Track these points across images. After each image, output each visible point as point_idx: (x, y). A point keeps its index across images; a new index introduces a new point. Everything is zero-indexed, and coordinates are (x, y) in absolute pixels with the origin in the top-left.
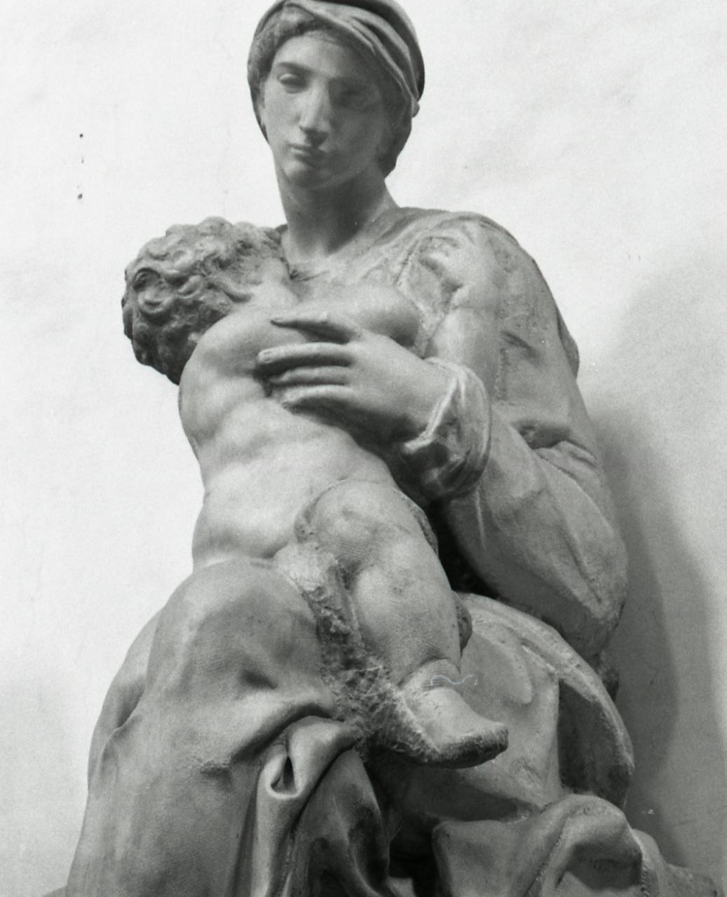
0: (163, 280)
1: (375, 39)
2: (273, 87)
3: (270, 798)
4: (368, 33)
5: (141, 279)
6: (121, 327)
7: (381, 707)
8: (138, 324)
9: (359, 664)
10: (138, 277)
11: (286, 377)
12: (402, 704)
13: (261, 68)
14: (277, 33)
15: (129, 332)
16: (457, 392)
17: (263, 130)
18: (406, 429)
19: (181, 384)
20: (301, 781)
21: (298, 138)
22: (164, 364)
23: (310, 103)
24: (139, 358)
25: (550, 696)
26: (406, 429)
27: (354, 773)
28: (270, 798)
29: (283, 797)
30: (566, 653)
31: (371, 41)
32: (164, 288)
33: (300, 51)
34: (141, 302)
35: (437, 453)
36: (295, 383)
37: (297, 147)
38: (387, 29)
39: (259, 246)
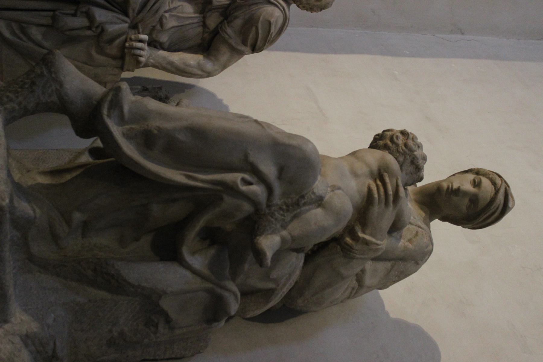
0: (405, 141)
1: (494, 210)
2: (471, 177)
3: (236, 177)
4: (496, 208)
5: (404, 133)
6: (386, 129)
7: (272, 219)
8: (389, 133)
9: (288, 211)
10: (405, 132)
11: (379, 183)
12: (413, 220)
13: (477, 172)
14: (491, 176)
15: (384, 131)
16: (378, 245)
17: (454, 175)
18: (364, 225)
19: (368, 149)
20: (244, 188)
21: (455, 186)
22: (375, 144)
23: (468, 187)
24: (376, 135)
25: (271, 285)
26: (364, 225)
27: (247, 208)
28: (236, 177)
29: (239, 182)
30: (285, 290)
31: (493, 209)
32: (403, 141)
33: (486, 182)
34: (397, 134)
35: (356, 238)
36: (377, 186)
37: (452, 186)
38: (496, 215)
39: (418, 174)
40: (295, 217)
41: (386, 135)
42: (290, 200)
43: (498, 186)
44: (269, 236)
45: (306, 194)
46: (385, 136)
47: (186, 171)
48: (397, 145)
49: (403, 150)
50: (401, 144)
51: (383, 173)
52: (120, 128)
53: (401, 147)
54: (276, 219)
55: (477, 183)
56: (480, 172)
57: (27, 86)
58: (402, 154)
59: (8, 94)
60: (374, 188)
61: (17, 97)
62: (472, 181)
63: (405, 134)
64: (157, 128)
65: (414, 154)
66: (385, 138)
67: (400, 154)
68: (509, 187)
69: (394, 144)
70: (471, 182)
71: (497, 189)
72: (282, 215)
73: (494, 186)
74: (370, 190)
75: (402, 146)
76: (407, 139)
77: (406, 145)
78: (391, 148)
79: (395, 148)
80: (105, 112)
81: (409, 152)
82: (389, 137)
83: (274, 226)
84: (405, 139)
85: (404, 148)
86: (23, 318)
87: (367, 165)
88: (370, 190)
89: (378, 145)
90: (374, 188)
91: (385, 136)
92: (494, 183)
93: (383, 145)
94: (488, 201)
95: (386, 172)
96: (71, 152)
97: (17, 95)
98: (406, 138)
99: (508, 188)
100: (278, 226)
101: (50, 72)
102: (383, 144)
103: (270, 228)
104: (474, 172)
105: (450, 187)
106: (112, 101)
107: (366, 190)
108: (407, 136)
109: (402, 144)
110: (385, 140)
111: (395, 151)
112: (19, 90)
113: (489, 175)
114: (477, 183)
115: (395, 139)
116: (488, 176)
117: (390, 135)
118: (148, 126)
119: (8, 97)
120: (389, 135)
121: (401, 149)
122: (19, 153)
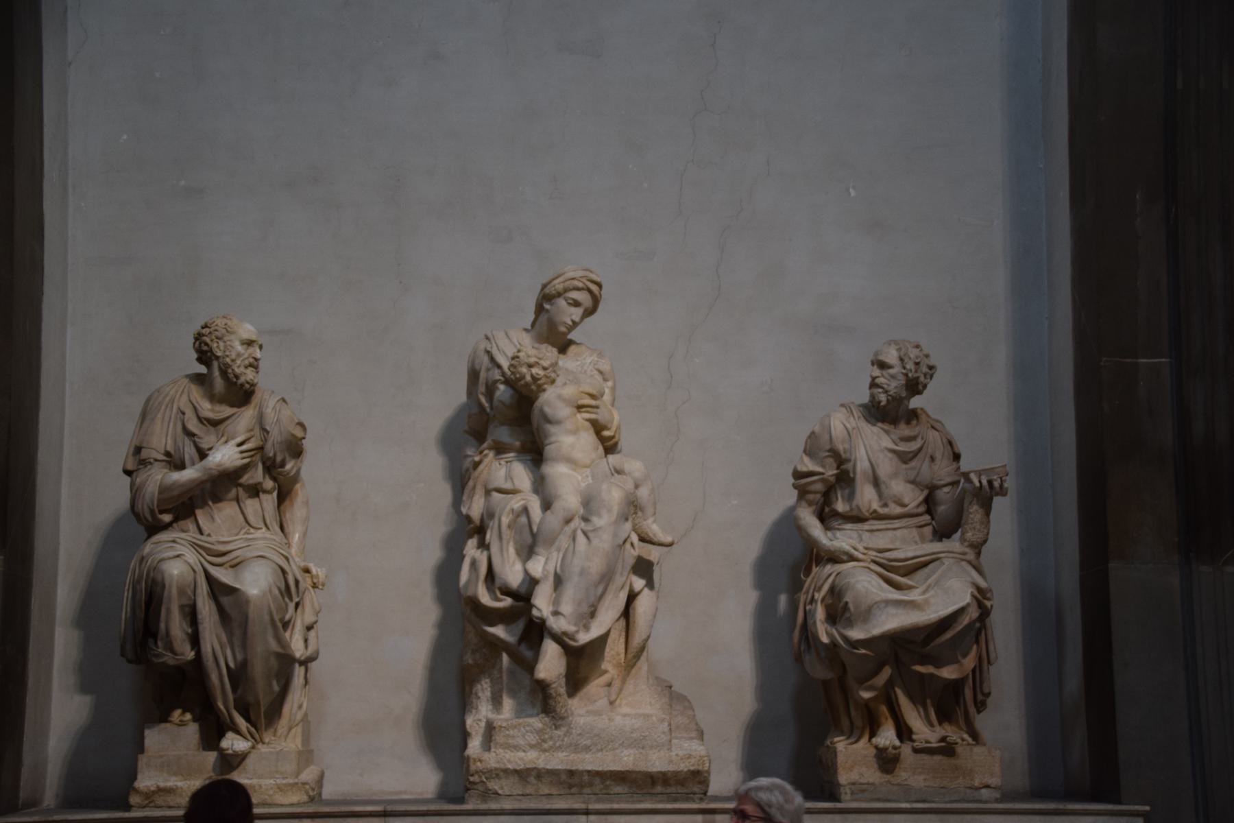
43: (585, 287)
74: (589, 420)
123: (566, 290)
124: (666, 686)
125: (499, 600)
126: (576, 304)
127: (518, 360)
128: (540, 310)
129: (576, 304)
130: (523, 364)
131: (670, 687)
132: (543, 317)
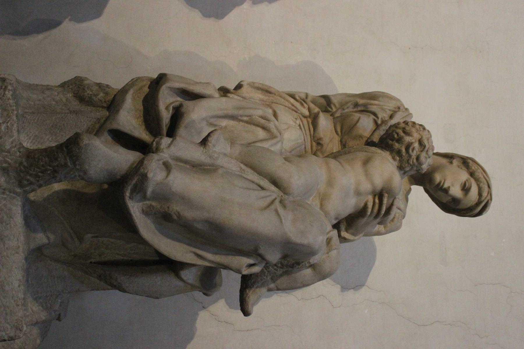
9: (281, 268)
10: (423, 143)
11: (377, 201)
40: (286, 273)
41: (405, 141)
42: (286, 262)
43: (483, 198)
44: (258, 290)
45: (302, 262)
46: (403, 141)
47: (195, 247)
48: (410, 156)
49: (413, 162)
50: (414, 156)
51: (384, 193)
52: (141, 204)
53: (412, 159)
54: (269, 272)
55: (466, 188)
56: (475, 175)
57: (49, 172)
58: (411, 165)
59: (28, 177)
60: (370, 205)
61: (38, 181)
62: (463, 184)
63: (422, 146)
64: (177, 213)
65: (421, 167)
66: (402, 143)
67: (409, 165)
68: (491, 200)
69: (407, 154)
70: (461, 184)
71: (480, 201)
72: (275, 269)
73: (479, 197)
74: (365, 206)
75: (413, 159)
76: (422, 151)
77: (418, 158)
78: (403, 157)
79: (406, 158)
80: (128, 194)
81: (418, 164)
82: (406, 143)
83: (265, 277)
84: (419, 150)
85: (415, 161)
86: (34, 308)
87: (373, 184)
88: (365, 206)
89: (393, 147)
90: (370, 205)
91: (403, 141)
92: (480, 194)
93: (398, 150)
94: (467, 207)
95: (387, 194)
96: (90, 117)
97: (37, 179)
98: (422, 149)
99: (490, 201)
100: (269, 278)
101: (74, 164)
102: (398, 148)
103: (262, 280)
104: (469, 171)
105: (442, 184)
106: (136, 186)
107: (362, 205)
108: (424, 147)
109: (415, 156)
110: (401, 145)
111: (406, 161)
112: (40, 174)
113: (481, 182)
114: (466, 188)
115: (410, 151)
116: (479, 183)
117: (408, 141)
118: (168, 208)
119: (28, 180)
120: (407, 141)
121: (411, 161)
122: (37, 118)
123: (477, 180)
124: (60, 314)
125: (167, 108)
126: (466, 189)
127: (422, 129)
128: (450, 157)
129: (466, 189)
130: (419, 134)
131: (59, 319)
132: (444, 161)
